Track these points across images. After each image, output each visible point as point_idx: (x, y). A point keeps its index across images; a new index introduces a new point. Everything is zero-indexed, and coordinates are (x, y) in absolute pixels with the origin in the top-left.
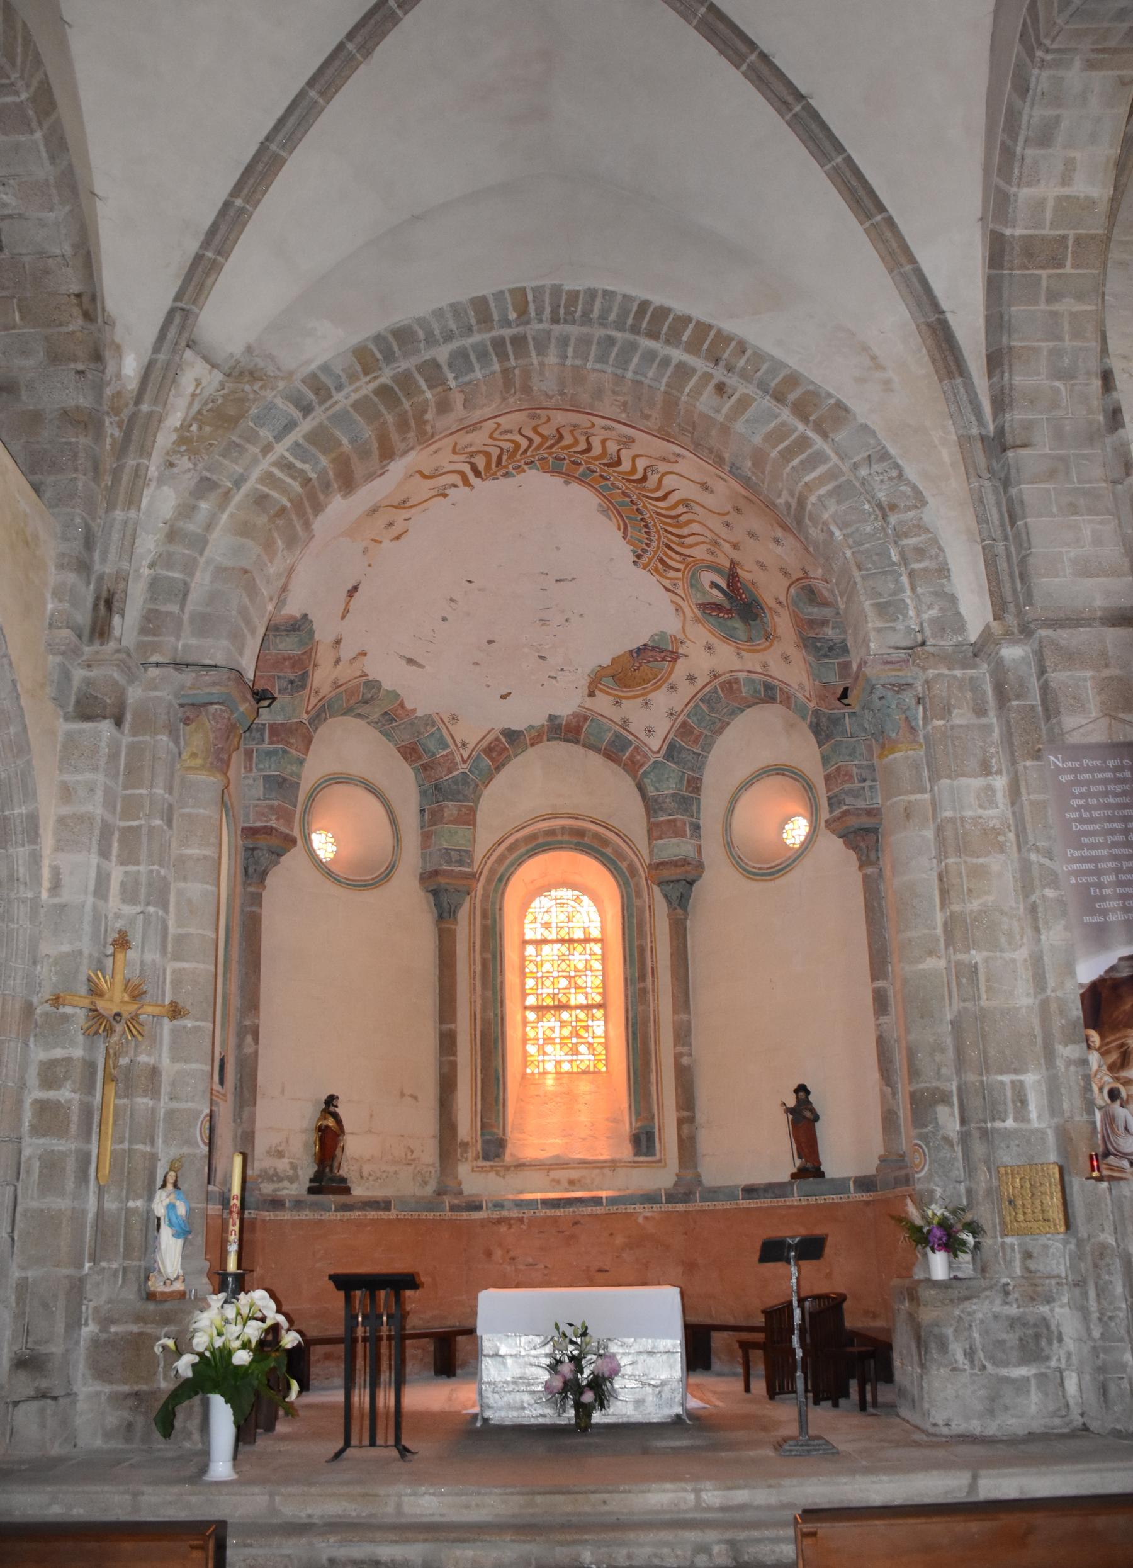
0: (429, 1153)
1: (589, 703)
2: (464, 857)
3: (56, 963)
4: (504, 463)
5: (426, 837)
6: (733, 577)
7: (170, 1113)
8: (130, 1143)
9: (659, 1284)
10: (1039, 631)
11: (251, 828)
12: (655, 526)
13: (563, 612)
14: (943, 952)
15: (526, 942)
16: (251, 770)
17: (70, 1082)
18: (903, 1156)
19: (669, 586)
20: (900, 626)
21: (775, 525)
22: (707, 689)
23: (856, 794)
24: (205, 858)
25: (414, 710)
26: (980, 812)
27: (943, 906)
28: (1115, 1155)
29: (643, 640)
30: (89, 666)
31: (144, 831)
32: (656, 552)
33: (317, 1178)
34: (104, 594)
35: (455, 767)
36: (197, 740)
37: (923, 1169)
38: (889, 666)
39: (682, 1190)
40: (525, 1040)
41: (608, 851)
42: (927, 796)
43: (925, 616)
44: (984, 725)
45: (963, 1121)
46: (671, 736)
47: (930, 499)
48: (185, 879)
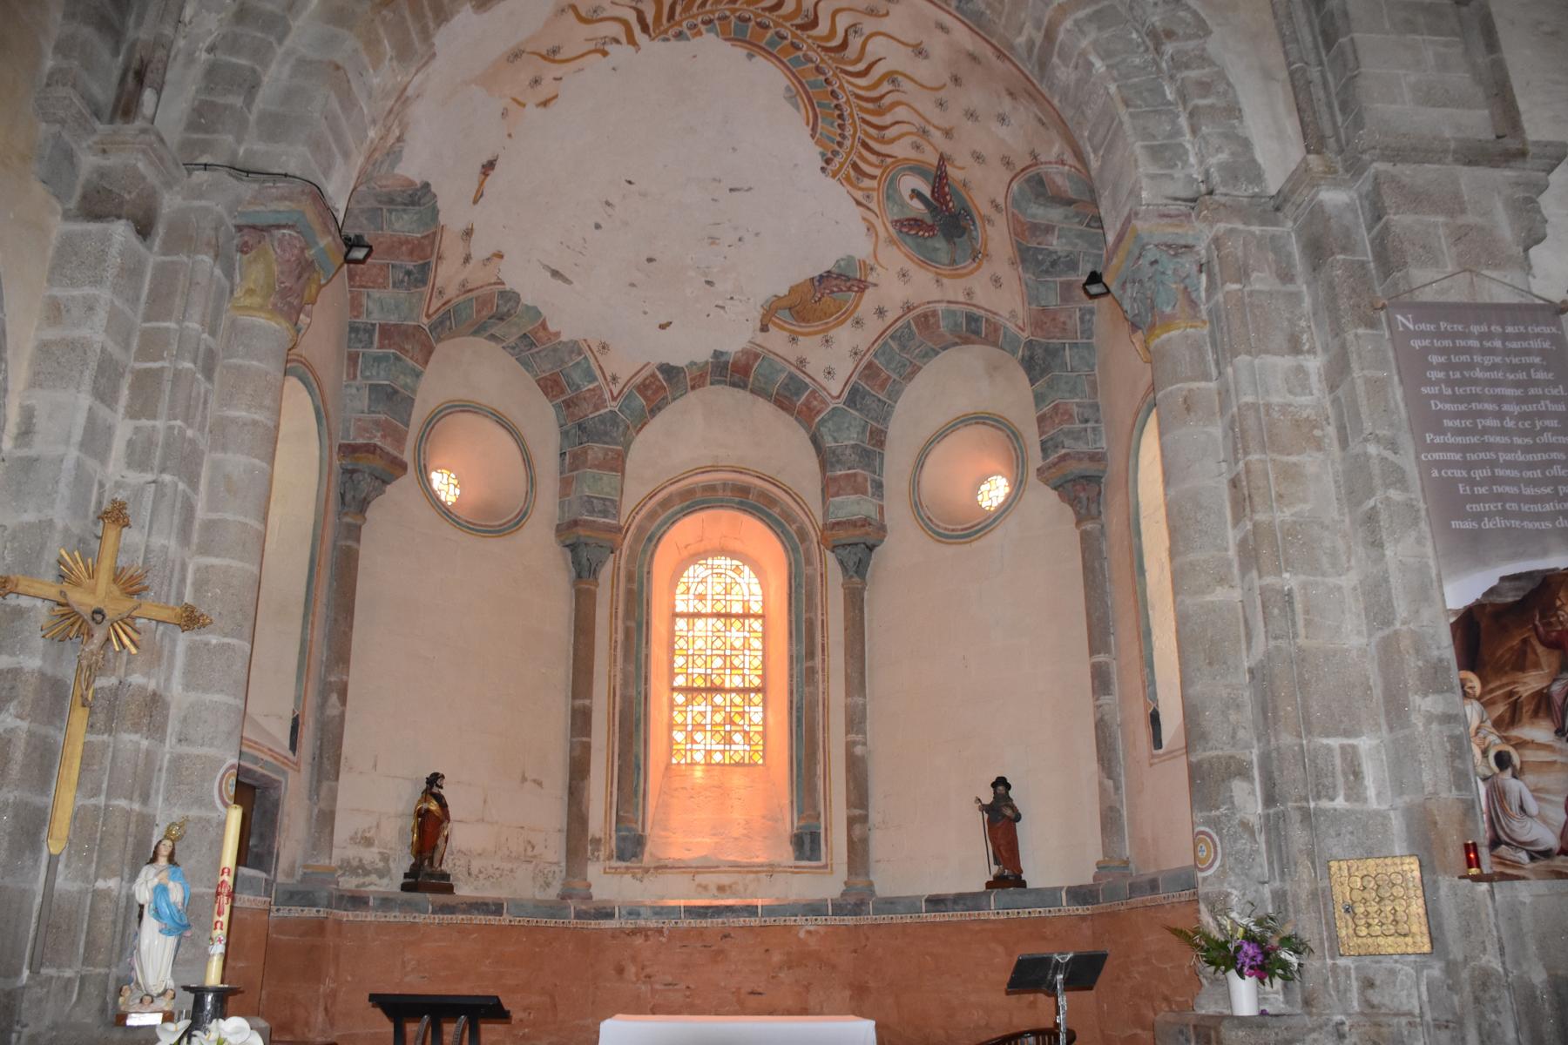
0: (553, 850)
1: (760, 338)
2: (610, 506)
3: (14, 538)
4: (677, 17)
5: (566, 484)
6: (940, 179)
7: (177, 760)
8: (108, 797)
9: (821, 1013)
10: (1375, 164)
11: (349, 445)
12: (851, 115)
13: (736, 229)
14: (1237, 581)
15: (676, 615)
16: (355, 377)
17: (15, 702)
18: (1127, 862)
19: (861, 199)
20: (1178, 173)
21: (1004, 93)
22: (899, 324)
23: (1077, 436)
24: (255, 423)
25: (557, 334)
26: (1290, 398)
27: (1237, 520)
28: (1507, 844)
29: (828, 265)
30: (104, 151)
31: (168, 375)
32: (848, 154)
33: (413, 873)
34: (135, 64)
35: (603, 403)
36: (255, 273)
37: (1211, 866)
38: (1166, 220)
39: (852, 900)
40: (671, 726)
41: (775, 512)
42: (1213, 385)
43: (1213, 161)
44: (1291, 294)
45: (1269, 800)
46: (854, 378)
47: (1215, 29)
48: (224, 449)
